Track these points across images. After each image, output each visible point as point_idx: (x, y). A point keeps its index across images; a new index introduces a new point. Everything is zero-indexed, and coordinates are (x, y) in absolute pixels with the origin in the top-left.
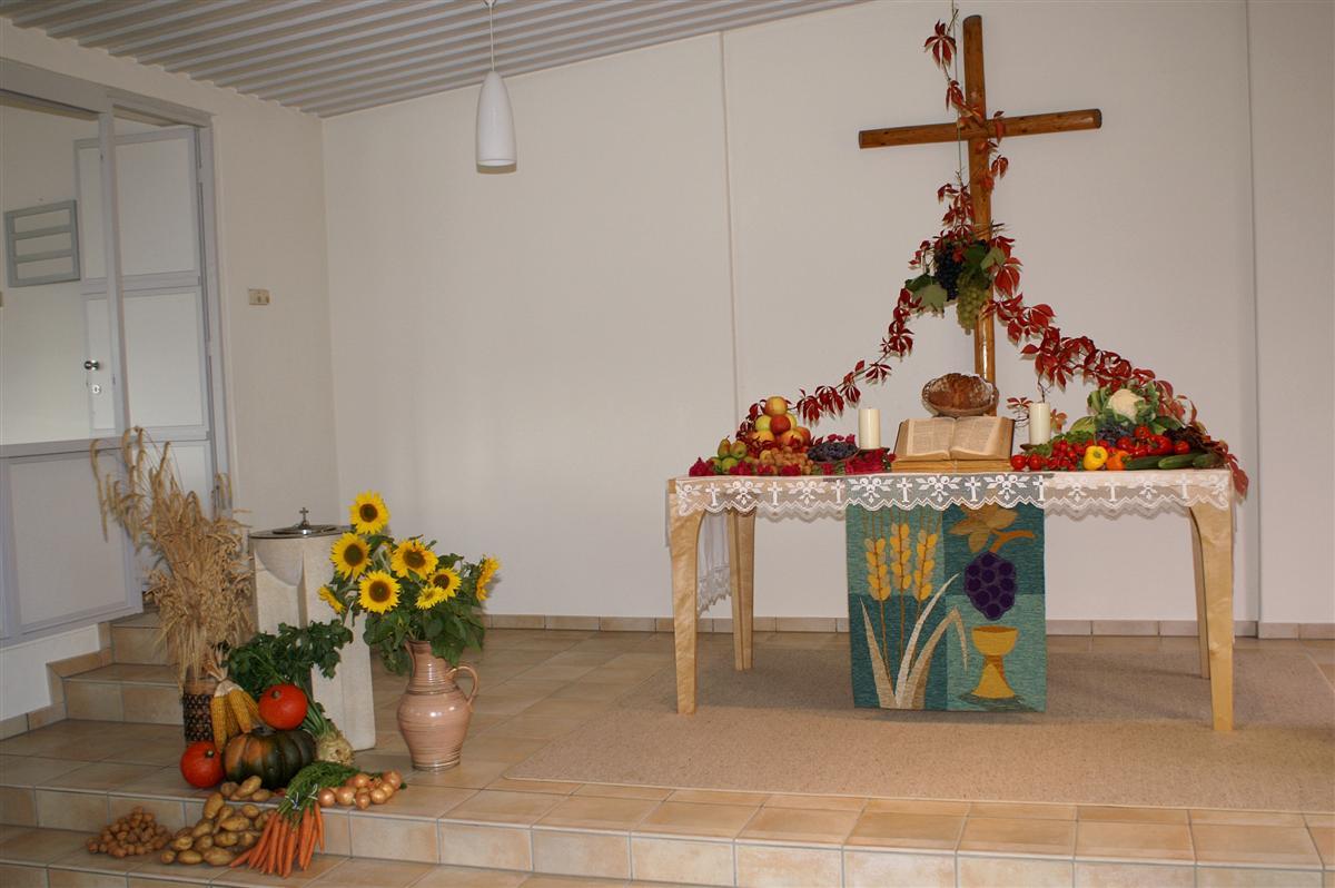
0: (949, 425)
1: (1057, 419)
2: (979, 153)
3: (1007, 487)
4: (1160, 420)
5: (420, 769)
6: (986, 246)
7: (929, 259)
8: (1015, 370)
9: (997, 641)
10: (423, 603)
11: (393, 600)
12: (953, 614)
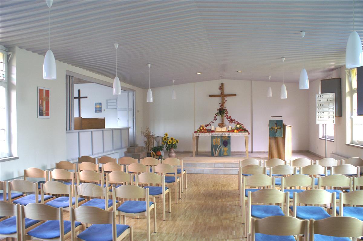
0: (220, 128)
1: (231, 128)
2: (223, 99)
3: (227, 134)
6: (224, 110)
8: (227, 122)
10: (173, 143)
12: (222, 146)
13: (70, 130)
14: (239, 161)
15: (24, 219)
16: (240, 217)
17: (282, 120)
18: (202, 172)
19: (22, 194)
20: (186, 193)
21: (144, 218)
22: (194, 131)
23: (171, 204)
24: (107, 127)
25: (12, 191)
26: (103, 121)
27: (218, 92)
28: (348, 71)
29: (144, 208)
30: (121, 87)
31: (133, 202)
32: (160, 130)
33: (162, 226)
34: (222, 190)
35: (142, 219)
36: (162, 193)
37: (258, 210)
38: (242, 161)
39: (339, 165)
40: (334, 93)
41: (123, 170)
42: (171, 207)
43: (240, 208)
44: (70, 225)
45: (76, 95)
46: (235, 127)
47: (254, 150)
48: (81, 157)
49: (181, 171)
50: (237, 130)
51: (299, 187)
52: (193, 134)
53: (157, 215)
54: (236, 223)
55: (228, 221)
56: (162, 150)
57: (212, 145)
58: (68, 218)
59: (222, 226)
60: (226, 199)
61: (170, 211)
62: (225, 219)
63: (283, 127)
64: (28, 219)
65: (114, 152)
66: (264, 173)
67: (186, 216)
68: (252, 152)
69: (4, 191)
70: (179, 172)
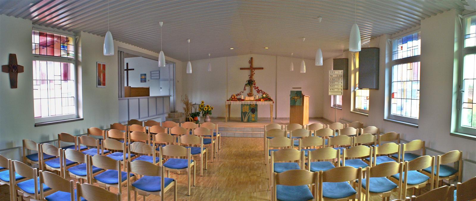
0: (249, 97)
1: (259, 97)
2: (252, 72)
3: (254, 103)
4: (267, 97)
5: (128, 158)
6: (253, 81)
7: (247, 82)
8: (254, 92)
9: (253, 116)
10: (209, 110)
11: (207, 110)
12: (250, 113)
13: (121, 97)
14: (264, 126)
15: (92, 166)
16: (265, 173)
17: (301, 91)
18: (233, 136)
19: (86, 147)
20: (220, 153)
21: (186, 173)
22: (227, 100)
23: (208, 163)
24: (151, 94)
25: (80, 144)
26: (148, 90)
27: (248, 65)
28: (353, 53)
29: (186, 165)
30: (166, 60)
31: (176, 159)
32: (197, 99)
33: (199, 181)
34: (250, 151)
35: (182, 175)
36: (200, 153)
37: (280, 166)
38: (267, 126)
39: (345, 127)
40: (343, 71)
41: (166, 132)
42: (208, 165)
43: (266, 166)
44: (125, 175)
45: (125, 68)
46: (262, 96)
47: (277, 117)
48: (130, 120)
49: (216, 134)
50: (263, 99)
51: (313, 146)
52: (226, 102)
53: (196, 172)
54: (262, 178)
55: (255, 177)
56: (199, 116)
57: (242, 112)
58: (124, 170)
59: (251, 181)
60: (254, 158)
61: (207, 169)
62: (253, 175)
63: (302, 97)
64: (94, 167)
65: (157, 117)
66: (285, 136)
67: (220, 173)
68: (276, 118)
69: (75, 144)
70: (215, 135)
